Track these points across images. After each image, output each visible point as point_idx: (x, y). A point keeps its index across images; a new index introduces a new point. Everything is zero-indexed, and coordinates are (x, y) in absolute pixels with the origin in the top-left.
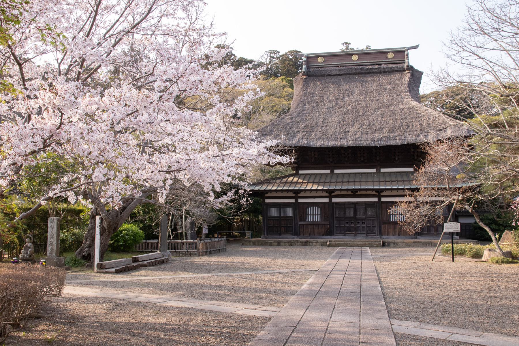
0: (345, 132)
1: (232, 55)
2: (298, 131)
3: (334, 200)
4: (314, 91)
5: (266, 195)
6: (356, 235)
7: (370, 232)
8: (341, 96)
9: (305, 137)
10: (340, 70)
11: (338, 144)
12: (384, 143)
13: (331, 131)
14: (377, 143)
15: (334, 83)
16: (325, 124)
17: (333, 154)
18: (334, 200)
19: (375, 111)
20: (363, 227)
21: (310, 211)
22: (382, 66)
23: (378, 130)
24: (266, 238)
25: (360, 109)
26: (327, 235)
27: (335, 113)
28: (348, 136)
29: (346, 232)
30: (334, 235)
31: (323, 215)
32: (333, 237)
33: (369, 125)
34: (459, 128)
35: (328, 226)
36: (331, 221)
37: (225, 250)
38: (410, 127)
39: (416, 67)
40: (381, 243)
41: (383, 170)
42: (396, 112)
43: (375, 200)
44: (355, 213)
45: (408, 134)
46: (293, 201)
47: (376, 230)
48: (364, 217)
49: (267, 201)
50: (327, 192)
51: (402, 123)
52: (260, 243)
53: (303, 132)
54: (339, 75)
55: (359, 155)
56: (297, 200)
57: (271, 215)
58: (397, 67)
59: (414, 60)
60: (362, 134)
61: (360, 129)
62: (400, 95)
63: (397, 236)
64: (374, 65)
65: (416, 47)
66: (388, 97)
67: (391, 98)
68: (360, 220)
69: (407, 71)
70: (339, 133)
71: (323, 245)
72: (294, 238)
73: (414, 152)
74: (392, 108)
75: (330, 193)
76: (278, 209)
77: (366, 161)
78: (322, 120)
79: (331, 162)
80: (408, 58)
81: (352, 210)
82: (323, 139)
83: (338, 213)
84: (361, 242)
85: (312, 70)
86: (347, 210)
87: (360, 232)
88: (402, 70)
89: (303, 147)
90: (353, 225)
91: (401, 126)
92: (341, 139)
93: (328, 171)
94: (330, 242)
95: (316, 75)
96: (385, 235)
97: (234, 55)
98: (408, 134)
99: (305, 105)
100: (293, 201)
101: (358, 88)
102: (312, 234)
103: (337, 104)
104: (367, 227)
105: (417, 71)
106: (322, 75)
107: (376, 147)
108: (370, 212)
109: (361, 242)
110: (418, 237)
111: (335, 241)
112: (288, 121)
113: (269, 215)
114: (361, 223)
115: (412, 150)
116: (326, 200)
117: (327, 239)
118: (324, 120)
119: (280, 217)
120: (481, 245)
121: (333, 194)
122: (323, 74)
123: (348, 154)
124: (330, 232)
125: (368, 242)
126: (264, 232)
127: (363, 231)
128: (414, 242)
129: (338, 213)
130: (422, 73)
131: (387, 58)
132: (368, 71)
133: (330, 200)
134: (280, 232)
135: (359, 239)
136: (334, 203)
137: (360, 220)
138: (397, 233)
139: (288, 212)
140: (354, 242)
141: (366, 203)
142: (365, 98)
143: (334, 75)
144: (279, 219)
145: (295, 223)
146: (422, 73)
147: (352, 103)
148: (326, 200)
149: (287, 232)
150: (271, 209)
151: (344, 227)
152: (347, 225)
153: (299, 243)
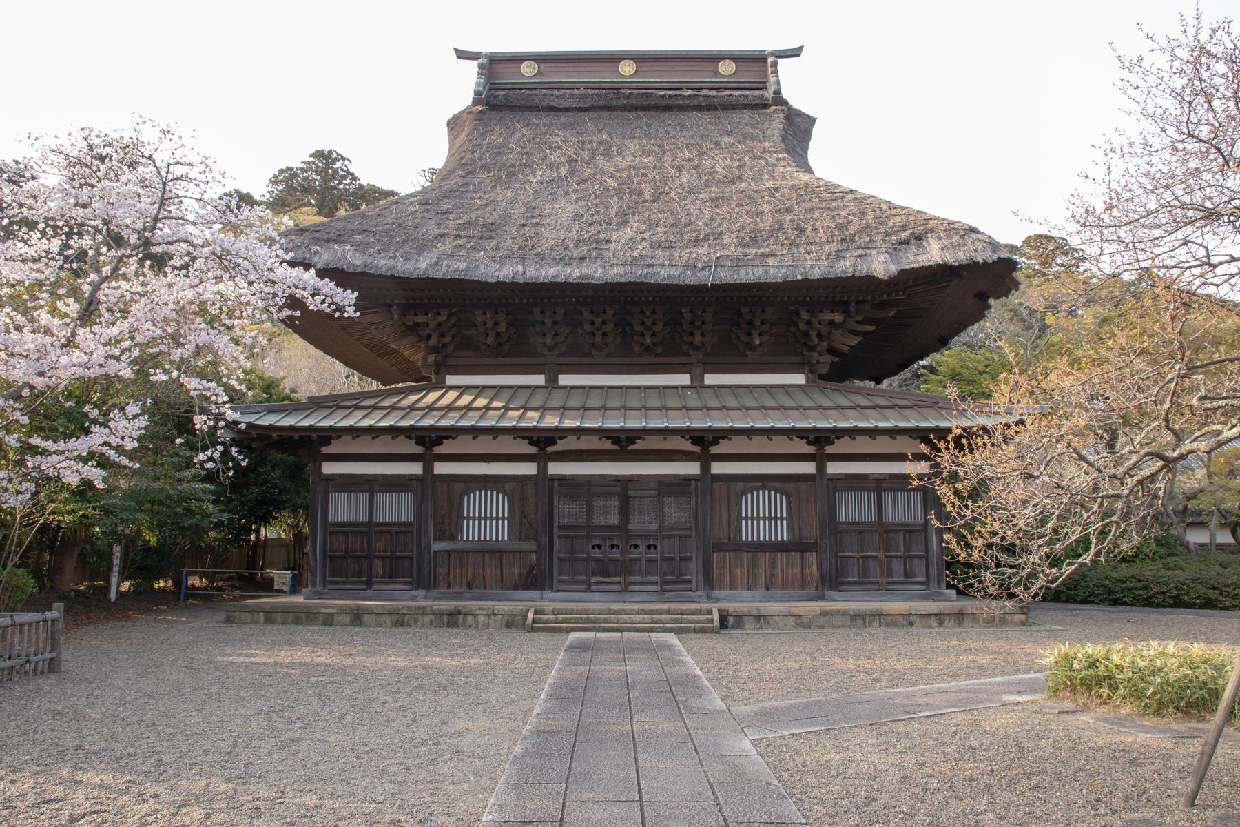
0: (598, 242)
1: (348, 172)
2: (442, 235)
3: (555, 469)
4: (505, 145)
5: (326, 450)
6: (625, 589)
7: (672, 579)
8: (586, 155)
9: (463, 252)
10: (582, 97)
11: (575, 273)
12: (725, 276)
13: (549, 239)
14: (705, 274)
15: (564, 127)
16: (533, 221)
17: (555, 323)
18: (555, 469)
19: (690, 192)
20: (649, 561)
21: (474, 504)
22: (705, 92)
23: (706, 238)
24: (320, 595)
25: (643, 186)
26: (526, 587)
27: (567, 193)
28: (606, 254)
29: (595, 579)
30: (551, 588)
31: (521, 522)
32: (548, 594)
33: (675, 225)
34: (962, 237)
35: (534, 557)
36: (545, 539)
37: (53, 666)
38: (809, 233)
39: (796, 103)
40: (716, 616)
41: (710, 379)
42: (756, 195)
43: (692, 469)
44: (625, 512)
45: (802, 250)
46: (415, 469)
47: (694, 570)
48: (655, 526)
49: (329, 469)
50: (532, 443)
51: (780, 223)
52: (290, 617)
53: (458, 236)
54: (580, 110)
55: (638, 328)
56: (428, 469)
57: (340, 519)
58: (746, 97)
59: (795, 85)
60: (652, 247)
61: (647, 235)
62: (761, 158)
63: (761, 592)
64: (679, 89)
65: (795, 53)
66: (728, 162)
67: (736, 163)
68: (640, 536)
69: (774, 107)
70: (578, 243)
71: (514, 623)
72: (414, 598)
73: (808, 322)
74: (743, 185)
75: (543, 442)
76: (364, 497)
77: (659, 349)
78: (523, 210)
79: (551, 349)
80: (776, 72)
81: (615, 503)
82: (523, 259)
83: (567, 512)
84: (645, 612)
85: (502, 93)
86: (598, 503)
87: (638, 578)
88: (762, 105)
89: (453, 281)
90: (616, 554)
91: (777, 229)
92: (583, 259)
93: (540, 380)
94: (536, 613)
95: (512, 108)
96: (721, 588)
97: (352, 174)
98: (802, 250)
99: (471, 173)
100: (415, 469)
101: (637, 141)
102: (475, 585)
103: (572, 172)
104: (664, 559)
105: (799, 114)
106: (534, 109)
107: (699, 289)
108: (675, 513)
109: (645, 612)
110: (829, 593)
111: (555, 612)
112: (411, 209)
113: (331, 517)
114: (643, 548)
115: (805, 316)
116: (529, 469)
117: (528, 602)
118: (530, 208)
119: (370, 524)
120: (1209, 641)
121: (550, 449)
122: (532, 104)
123: (604, 323)
124: (536, 579)
125: (669, 612)
126: (314, 575)
127: (648, 574)
128: (823, 614)
129: (567, 512)
130: (814, 120)
131: (717, 73)
132: (664, 103)
133: (543, 469)
134: (370, 576)
135: (636, 604)
136: (553, 479)
137: (640, 536)
138: (762, 581)
139: (398, 509)
140: (620, 612)
141: (661, 481)
142: (660, 160)
143: (567, 110)
144: (368, 529)
145: (419, 545)
146: (814, 120)
147: (618, 171)
148: (529, 469)
149: (391, 575)
150: (341, 495)
151: (585, 560)
152: (597, 554)
153: (427, 618)
